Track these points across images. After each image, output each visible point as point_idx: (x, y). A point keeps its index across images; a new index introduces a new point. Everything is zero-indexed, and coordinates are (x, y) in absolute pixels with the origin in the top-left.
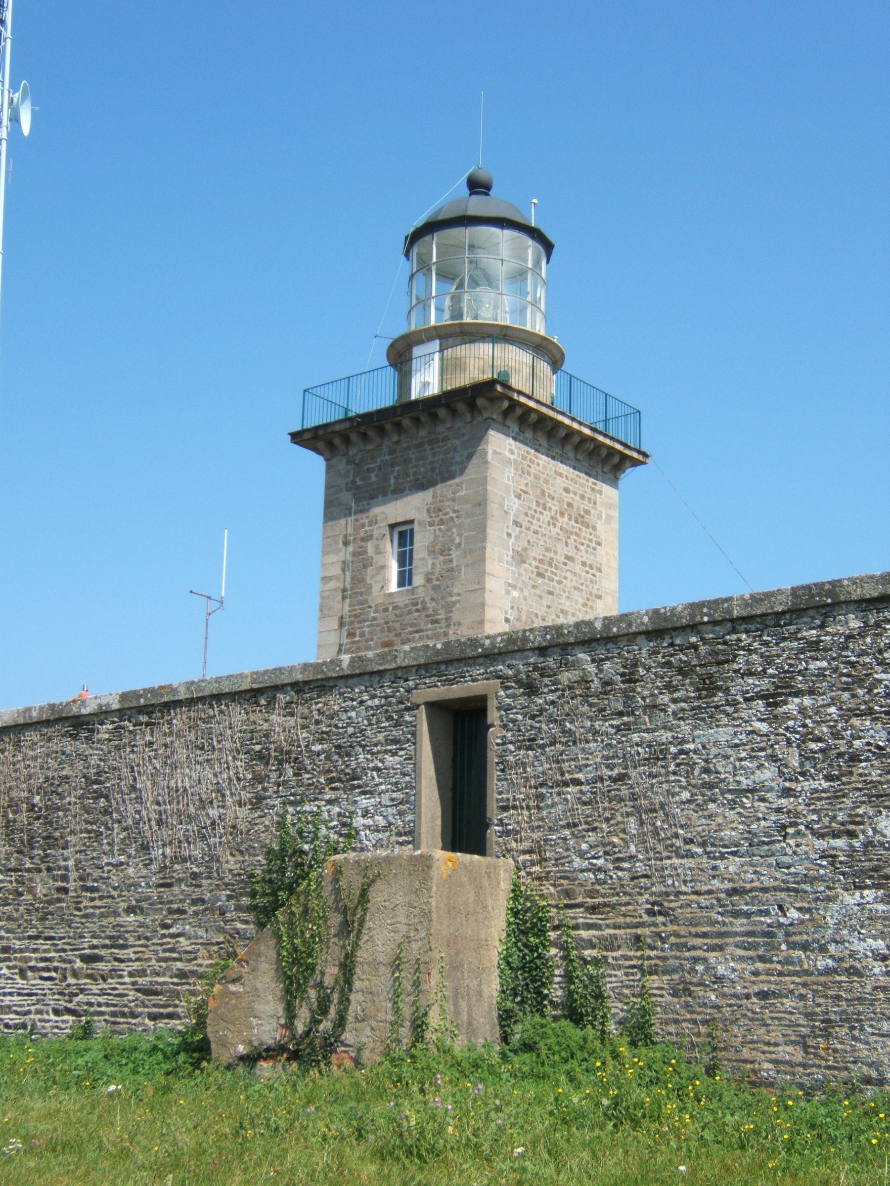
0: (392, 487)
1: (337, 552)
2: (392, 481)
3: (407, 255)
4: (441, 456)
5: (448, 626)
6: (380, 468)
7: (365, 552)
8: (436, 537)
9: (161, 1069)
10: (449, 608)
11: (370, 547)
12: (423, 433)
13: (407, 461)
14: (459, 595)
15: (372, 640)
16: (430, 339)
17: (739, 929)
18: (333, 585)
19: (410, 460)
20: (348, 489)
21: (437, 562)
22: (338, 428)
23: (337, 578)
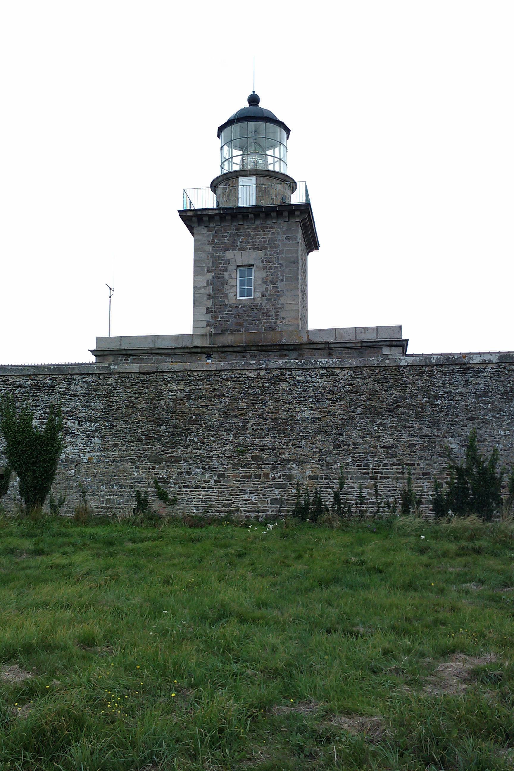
0: (239, 247)
1: (204, 275)
2: (239, 244)
3: (219, 136)
4: (270, 236)
5: (277, 319)
6: (230, 236)
7: (223, 277)
8: (267, 276)
9: (417, 662)
10: (277, 309)
11: (226, 275)
12: (258, 222)
13: (249, 235)
14: (282, 304)
15: (229, 321)
16: (251, 175)
17: (41, 376)
18: (202, 291)
19: (250, 235)
20: (210, 244)
21: (269, 287)
22: (210, 212)
23: (204, 288)
